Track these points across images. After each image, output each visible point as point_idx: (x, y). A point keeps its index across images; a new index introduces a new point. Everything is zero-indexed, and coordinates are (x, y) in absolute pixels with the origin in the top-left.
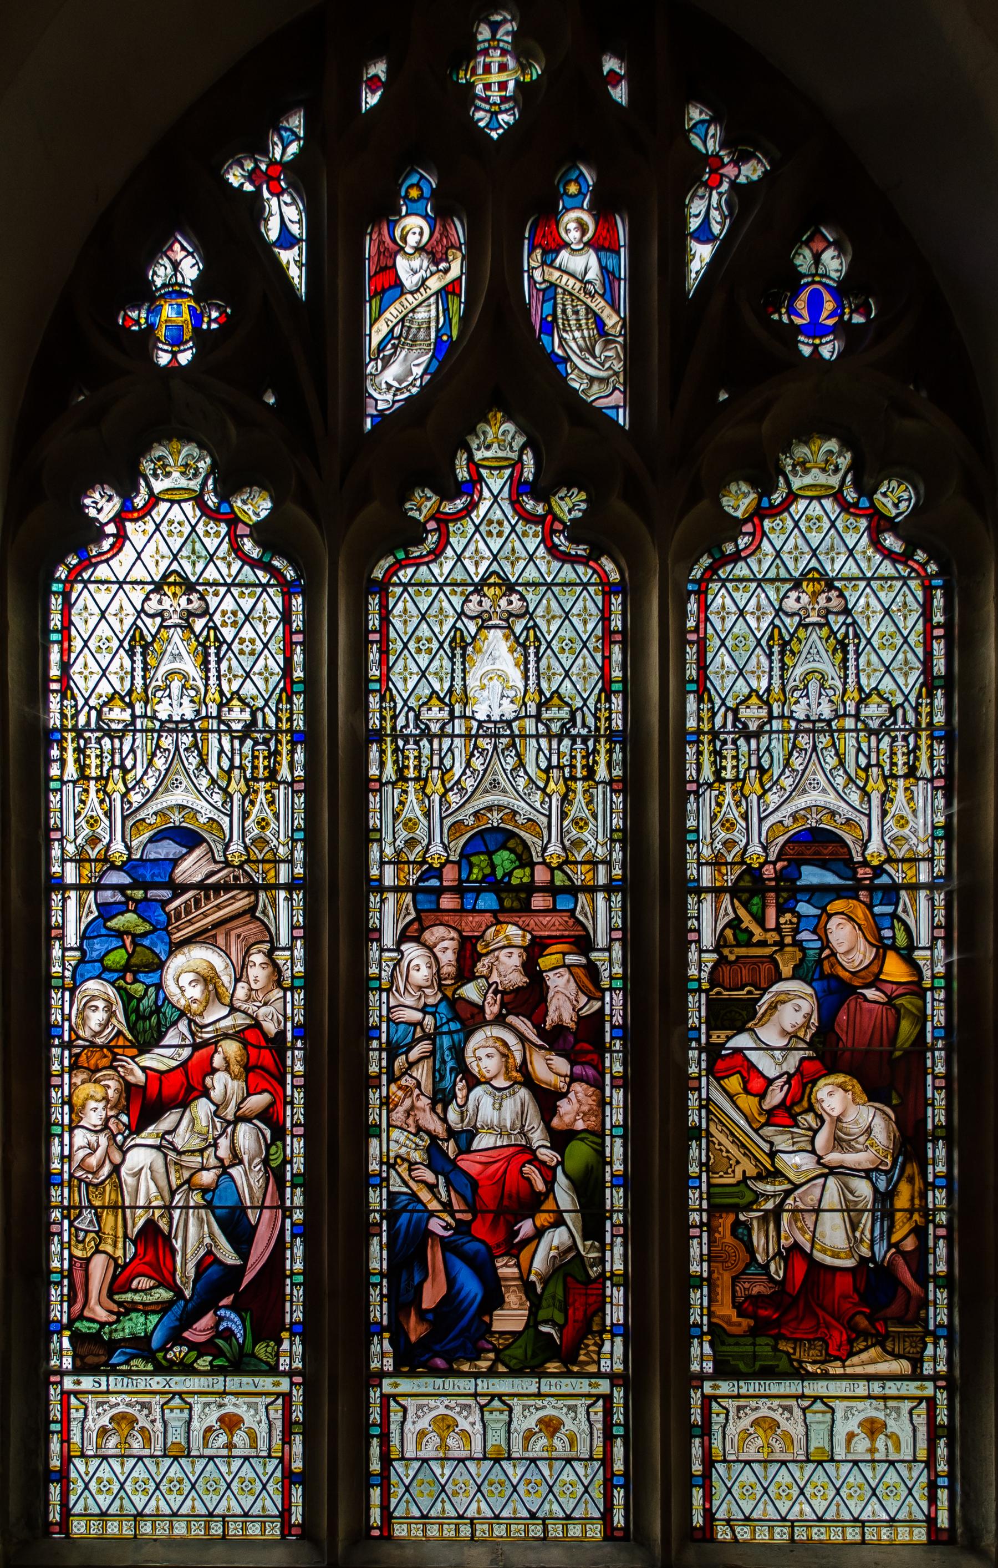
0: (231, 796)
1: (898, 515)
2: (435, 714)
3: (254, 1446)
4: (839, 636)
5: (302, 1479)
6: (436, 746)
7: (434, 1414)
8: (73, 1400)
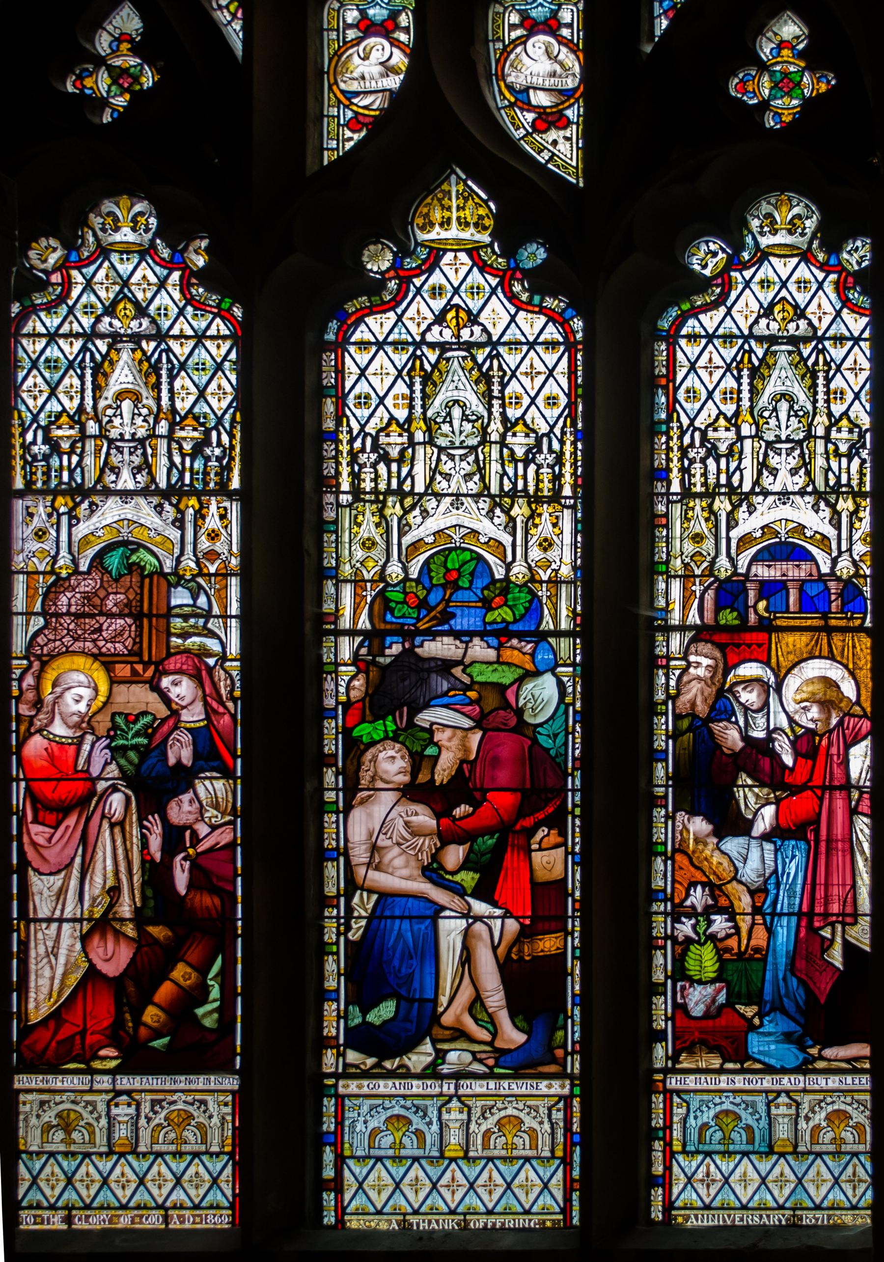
0: (839, 514)
1: (724, 251)
2: (64, 433)
3: (534, 1146)
4: (810, 363)
5: (653, 1181)
6: (723, 465)
7: (389, 1113)
8: (676, 1099)
